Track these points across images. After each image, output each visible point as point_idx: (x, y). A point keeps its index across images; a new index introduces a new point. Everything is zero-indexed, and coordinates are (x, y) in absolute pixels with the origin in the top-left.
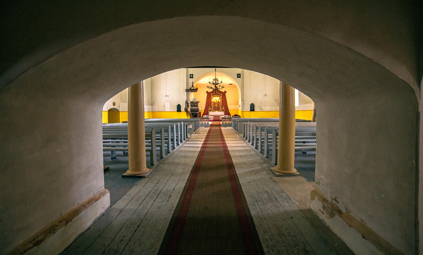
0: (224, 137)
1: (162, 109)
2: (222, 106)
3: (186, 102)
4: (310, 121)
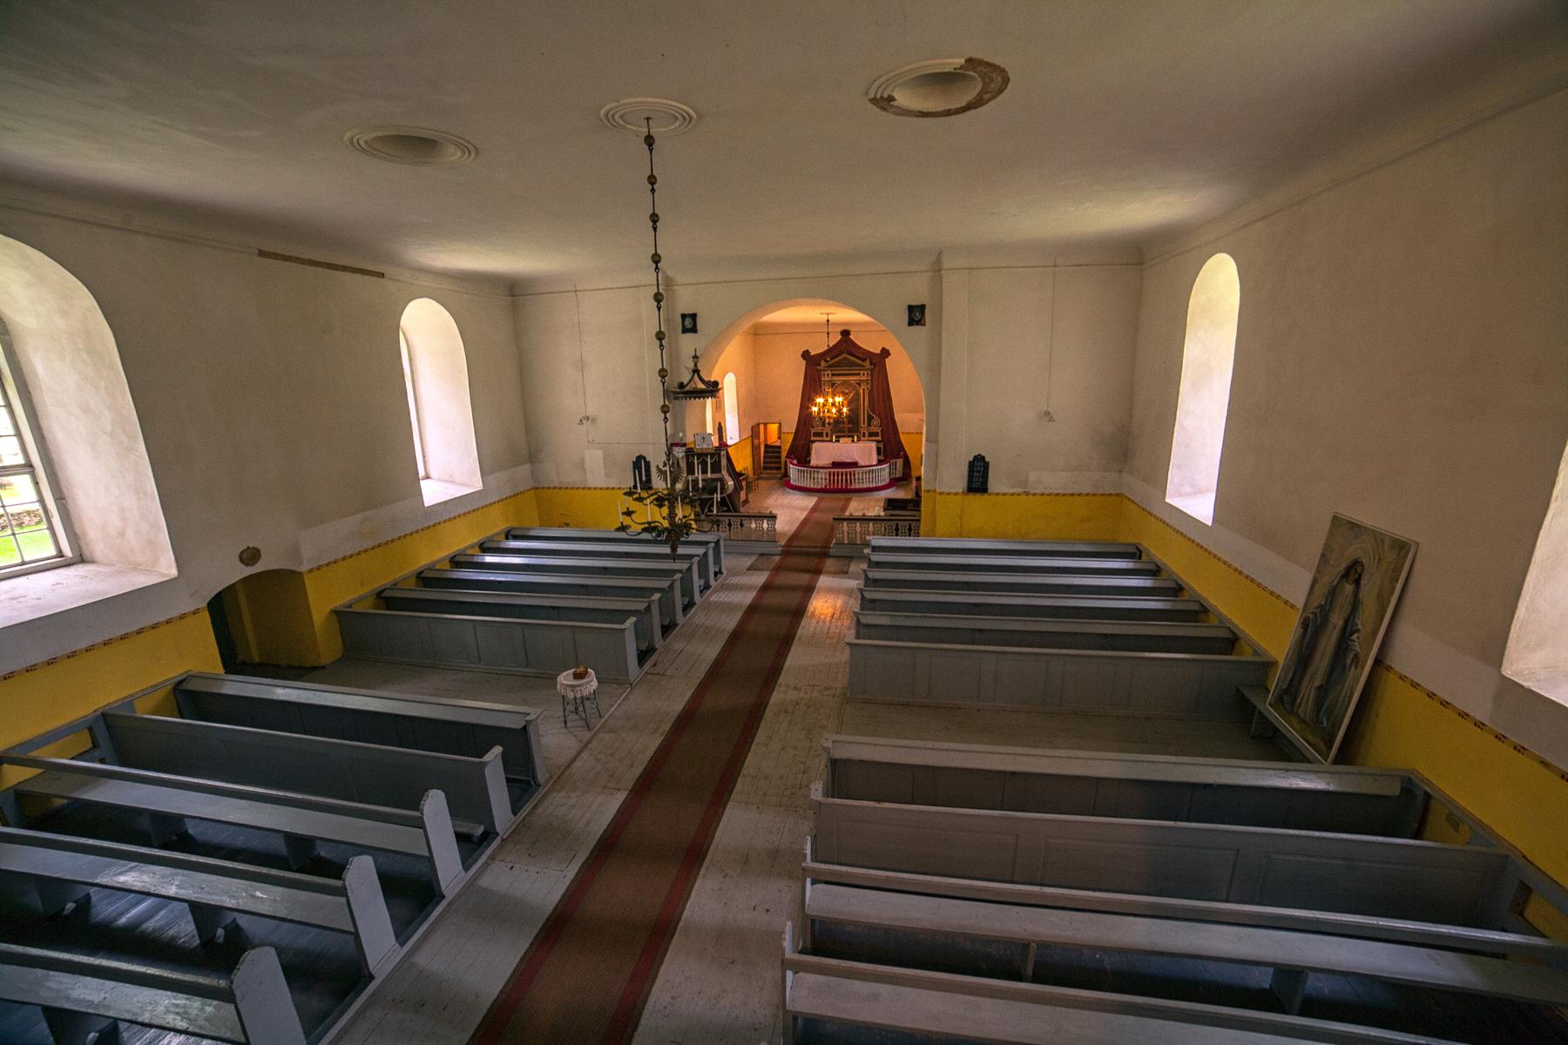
2: (869, 416)
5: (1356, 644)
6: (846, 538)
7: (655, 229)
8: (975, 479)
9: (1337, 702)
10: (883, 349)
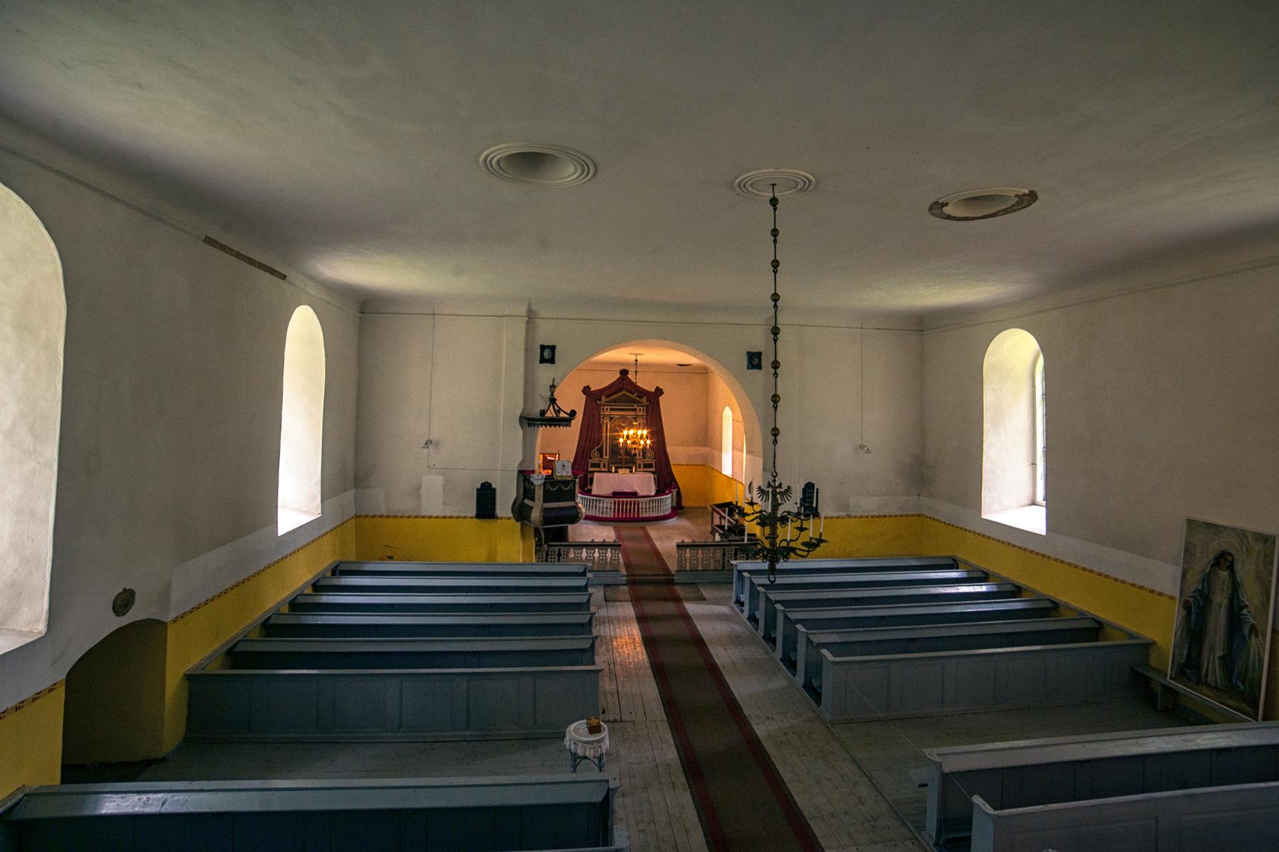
3: (520, 472)
5: (1249, 617)
6: (688, 564)
7: (775, 273)
9: (1247, 670)
10: (658, 388)
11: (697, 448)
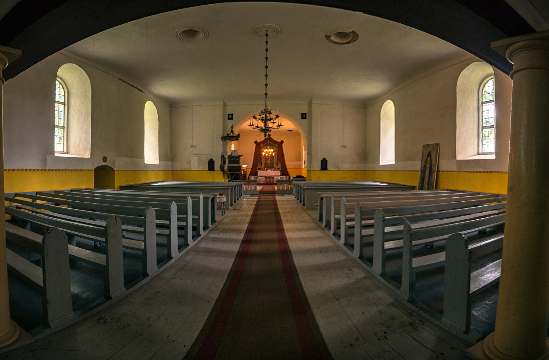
0: (282, 218)
1: (186, 167)
2: (277, 162)
4: (413, 188)
8: (323, 166)
11: (297, 162)
